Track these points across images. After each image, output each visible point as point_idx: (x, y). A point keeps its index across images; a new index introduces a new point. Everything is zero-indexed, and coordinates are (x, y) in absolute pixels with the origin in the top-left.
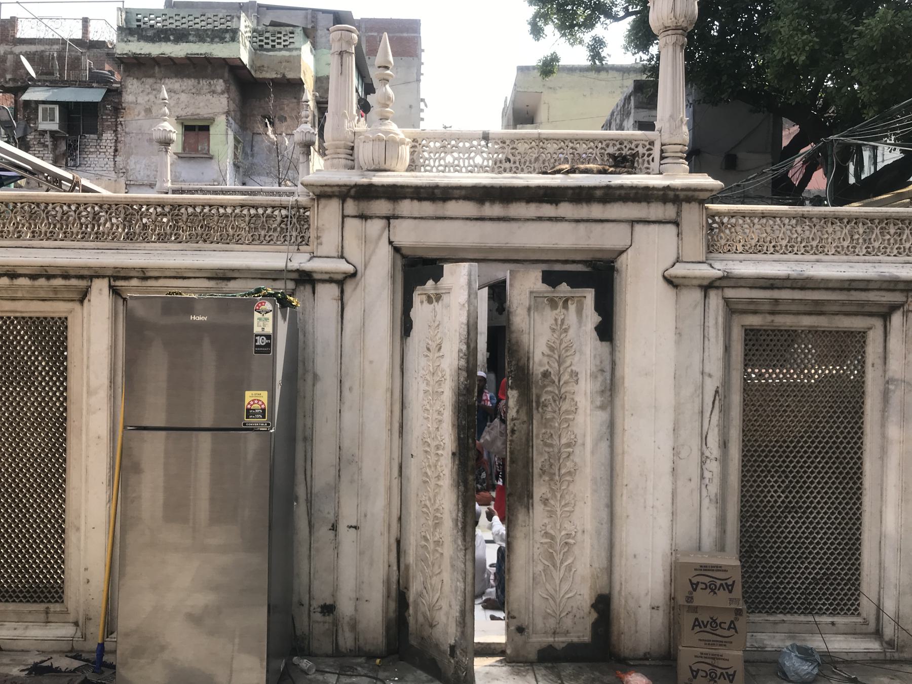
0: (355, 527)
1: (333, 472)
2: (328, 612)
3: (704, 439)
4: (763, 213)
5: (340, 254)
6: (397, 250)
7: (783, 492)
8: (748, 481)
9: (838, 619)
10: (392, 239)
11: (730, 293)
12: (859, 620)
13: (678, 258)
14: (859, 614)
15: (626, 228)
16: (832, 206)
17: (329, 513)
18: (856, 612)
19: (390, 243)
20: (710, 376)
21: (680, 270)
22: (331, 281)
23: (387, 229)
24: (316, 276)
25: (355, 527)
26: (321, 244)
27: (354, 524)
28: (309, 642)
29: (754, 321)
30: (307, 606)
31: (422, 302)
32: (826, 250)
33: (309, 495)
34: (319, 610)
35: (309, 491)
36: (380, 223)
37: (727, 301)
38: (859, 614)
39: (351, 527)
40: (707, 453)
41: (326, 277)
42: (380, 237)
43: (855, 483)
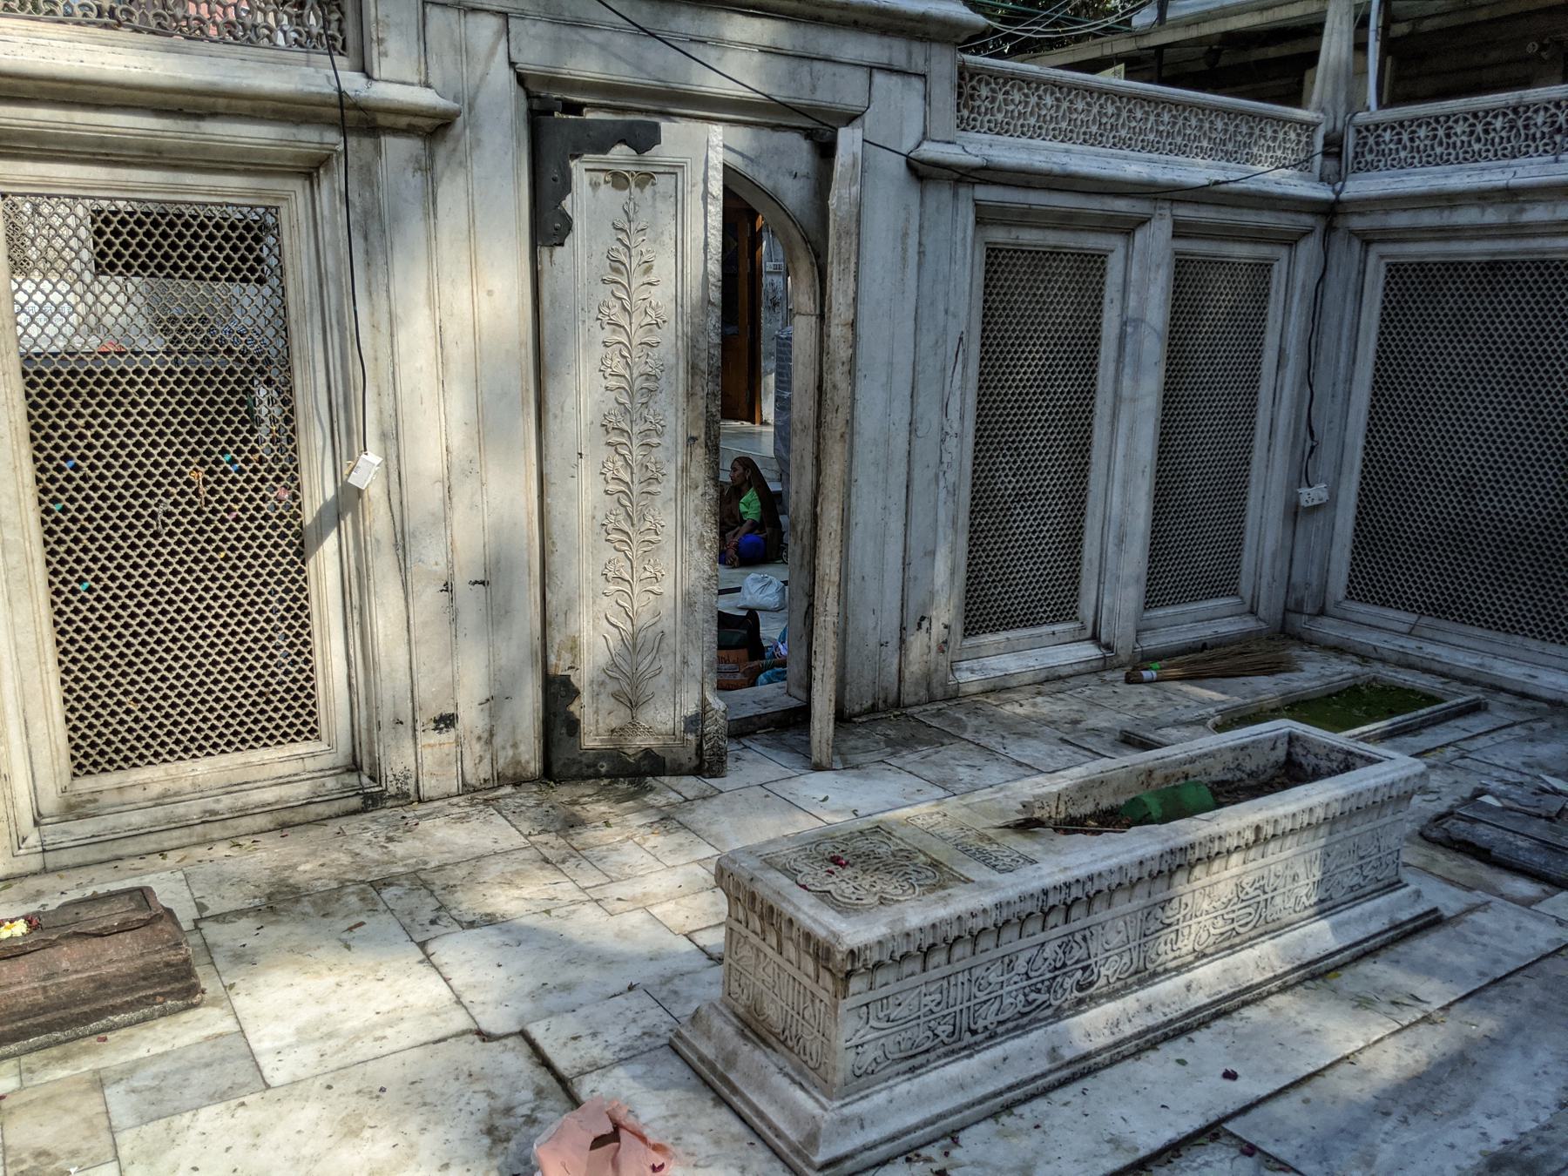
0: (483, 583)
1: (438, 492)
2: (447, 726)
3: (945, 408)
4: (1013, 74)
5: (423, 79)
6: (521, 79)
7: (1014, 476)
8: (979, 464)
9: (1058, 628)
10: (515, 58)
11: (982, 193)
12: (1078, 625)
13: (925, 133)
14: (1077, 619)
15: (860, 76)
16: (1126, 78)
17: (437, 564)
18: (1235, 593)
19: (512, 64)
20: (955, 316)
21: (931, 151)
22: (409, 131)
23: (504, 39)
24: (382, 120)
25: (483, 583)
26: (386, 54)
27: (480, 578)
28: (417, 781)
29: (1389, 261)
30: (409, 722)
31: (595, 185)
32: (978, 124)
33: (399, 536)
34: (433, 725)
35: (398, 529)
36: (493, 23)
37: (978, 206)
38: (1077, 619)
39: (476, 582)
40: (947, 429)
41: (403, 121)
42: (492, 53)
43: (1083, 457)
